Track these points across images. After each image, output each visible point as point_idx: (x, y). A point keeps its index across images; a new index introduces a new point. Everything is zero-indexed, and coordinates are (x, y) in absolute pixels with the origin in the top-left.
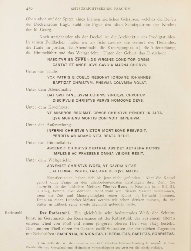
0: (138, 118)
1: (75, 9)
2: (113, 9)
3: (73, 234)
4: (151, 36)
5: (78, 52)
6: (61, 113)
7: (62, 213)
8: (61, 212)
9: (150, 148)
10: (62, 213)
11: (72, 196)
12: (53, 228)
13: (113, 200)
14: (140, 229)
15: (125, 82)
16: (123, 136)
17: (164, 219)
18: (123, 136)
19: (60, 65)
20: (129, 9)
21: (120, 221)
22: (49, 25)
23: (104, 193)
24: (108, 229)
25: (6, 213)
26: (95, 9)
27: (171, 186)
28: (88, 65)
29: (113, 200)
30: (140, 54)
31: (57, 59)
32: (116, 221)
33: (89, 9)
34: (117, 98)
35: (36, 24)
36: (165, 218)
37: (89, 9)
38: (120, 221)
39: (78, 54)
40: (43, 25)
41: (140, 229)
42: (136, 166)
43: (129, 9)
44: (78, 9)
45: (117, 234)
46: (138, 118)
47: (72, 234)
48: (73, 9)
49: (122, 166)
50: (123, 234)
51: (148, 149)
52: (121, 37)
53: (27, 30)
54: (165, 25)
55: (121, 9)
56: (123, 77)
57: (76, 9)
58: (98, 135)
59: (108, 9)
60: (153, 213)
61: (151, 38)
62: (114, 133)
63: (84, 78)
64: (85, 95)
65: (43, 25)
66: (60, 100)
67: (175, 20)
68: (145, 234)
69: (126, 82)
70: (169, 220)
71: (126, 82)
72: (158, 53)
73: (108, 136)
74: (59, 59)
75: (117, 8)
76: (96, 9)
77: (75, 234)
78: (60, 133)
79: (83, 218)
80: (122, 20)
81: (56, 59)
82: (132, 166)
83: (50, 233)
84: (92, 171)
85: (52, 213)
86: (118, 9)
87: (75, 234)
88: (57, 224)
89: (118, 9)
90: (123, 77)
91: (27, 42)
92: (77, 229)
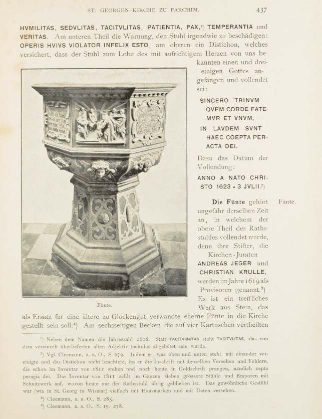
3: (174, 27)
5: (201, 306)
6: (64, 28)
9: (153, 27)
11: (266, 27)
12: (221, 228)
15: (31, 27)
16: (68, 28)
18: (68, 27)
19: (241, 28)
20: (196, 10)
28: (122, 45)
31: (113, 27)
39: (202, 309)
43: (196, 10)
45: (234, 27)
47: (171, 27)
49: (251, 27)
50: (129, 27)
51: (189, 28)
55: (182, 10)
56: (238, 27)
58: (85, 26)
63: (119, 46)
64: (29, 28)
66: (111, 27)
68: (46, 28)
69: (220, 25)
71: (220, 25)
72: (107, 326)
73: (219, 264)
74: (115, 27)
77: (176, 27)
81: (111, 27)
82: (134, 28)
83: (261, 324)
84: (104, 27)
87: (176, 27)
88: (236, 54)
90: (238, 27)
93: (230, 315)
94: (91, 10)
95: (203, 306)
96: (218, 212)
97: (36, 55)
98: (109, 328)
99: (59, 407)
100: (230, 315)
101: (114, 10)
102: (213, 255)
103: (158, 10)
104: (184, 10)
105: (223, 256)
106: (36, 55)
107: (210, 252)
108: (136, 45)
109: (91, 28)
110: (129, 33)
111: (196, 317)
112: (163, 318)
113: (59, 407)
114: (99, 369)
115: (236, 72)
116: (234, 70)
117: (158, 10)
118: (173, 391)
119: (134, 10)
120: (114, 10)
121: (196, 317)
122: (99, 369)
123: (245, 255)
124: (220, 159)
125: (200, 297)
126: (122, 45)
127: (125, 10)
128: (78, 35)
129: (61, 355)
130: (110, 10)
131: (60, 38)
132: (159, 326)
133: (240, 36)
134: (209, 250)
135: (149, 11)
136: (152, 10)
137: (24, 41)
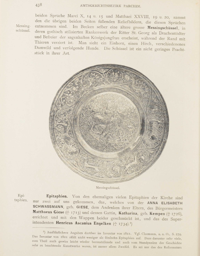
2: (122, 6)
4: (174, 49)
5: (80, 217)
6: (85, 207)
8: (157, 27)
13: (40, 21)
17: (121, 28)
20: (139, 6)
21: (125, 25)
23: (68, 24)
26: (104, 6)
27: (145, 16)
28: (165, 203)
29: (40, 21)
32: (122, 25)
33: (98, 6)
35: (36, 47)
36: (122, 27)
37: (98, 6)
38: (125, 25)
39: (81, 218)
42: (88, 207)
44: (88, 6)
48: (82, 6)
53: (84, 197)
54: (94, 38)
55: (130, 6)
57: (86, 6)
59: (117, 6)
60: (36, 21)
61: (174, 50)
63: (164, 203)
67: (17, 31)
70: (112, 29)
75: (126, 6)
76: (106, 6)
79: (157, 27)
88: (131, 203)
89: (128, 6)
91: (74, 27)
93: (183, 28)
95: (82, 217)
97: (128, 219)
98: (139, 51)
99: (173, 248)
100: (183, 28)
104: (132, 6)
105: (96, 197)
106: (178, 23)
108: (83, 207)
109: (47, 207)
113: (173, 248)
114: (127, 234)
122: (127, 234)
125: (130, 196)
126: (165, 203)
128: (177, 208)
129: (143, 234)
131: (104, 208)
135: (134, 7)
137: (182, 47)
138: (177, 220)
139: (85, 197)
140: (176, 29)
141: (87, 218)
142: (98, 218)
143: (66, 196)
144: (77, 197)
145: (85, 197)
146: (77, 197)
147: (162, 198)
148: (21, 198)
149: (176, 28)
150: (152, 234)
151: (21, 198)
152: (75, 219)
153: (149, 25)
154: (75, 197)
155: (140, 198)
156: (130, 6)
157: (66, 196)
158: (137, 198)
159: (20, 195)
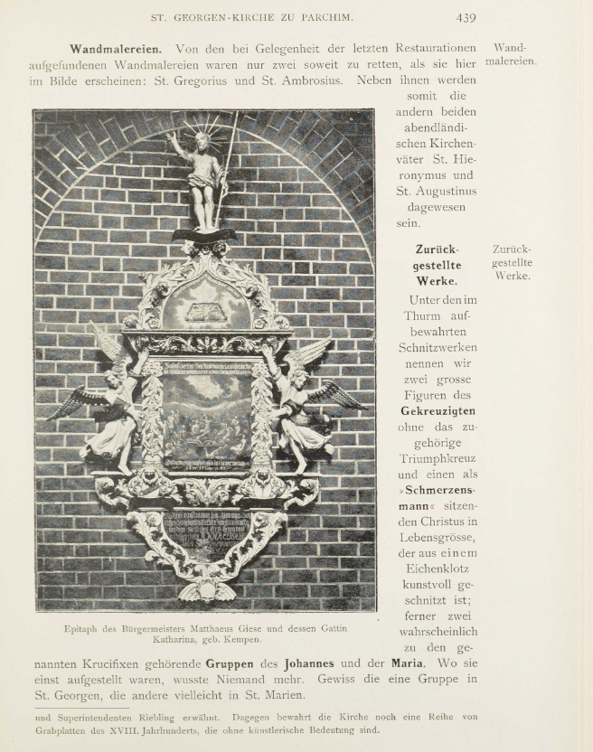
0: (462, 208)
1: (444, 717)
5: (442, 661)
7: (460, 410)
10: (460, 410)
14: (440, 523)
20: (347, 17)
22: (453, 459)
24: (437, 161)
25: (431, 717)
29: (458, 364)
30: (438, 428)
34: (174, 635)
38: (424, 593)
39: (444, 665)
40: (464, 348)
41: (440, 523)
43: (347, 17)
46: (462, 208)
52: (291, 82)
53: (457, 396)
62: (279, 725)
65: (464, 348)
75: (309, 16)
78: (199, 688)
80: (178, 82)
85: (435, 717)
86: (315, 19)
89: (315, 19)
92: (471, 301)
94: (158, 18)
96: (163, 66)
101: (199, 18)
102: (438, 143)
103: (278, 17)
105: (161, 665)
107: (434, 137)
110: (501, 43)
111: (418, 617)
112: (137, 682)
115: (456, 570)
116: (63, 694)
117: (278, 17)
118: (337, 664)
119: (222, 17)
120: (199, 18)
121: (418, 617)
123: (436, 49)
124: (411, 208)
125: (410, 566)
127: (218, 17)
130: (192, 18)
132: (83, 732)
133: (413, 601)
134: (442, 655)
136: (267, 18)
138: (449, 680)
139: (210, 49)
140: (442, 267)
141: (442, 680)
142: (445, 113)
143: (155, 50)
144: (189, 50)
145: (210, 49)
146: (189, 50)
147: (141, 718)
148: (402, 492)
149: (442, 264)
150: (440, 250)
151: (402, 492)
152: (443, 652)
153: (442, 655)
154: (183, 51)
155: (437, 460)
156: (321, 18)
157: (155, 50)
158: (433, 349)
159: (70, 629)
